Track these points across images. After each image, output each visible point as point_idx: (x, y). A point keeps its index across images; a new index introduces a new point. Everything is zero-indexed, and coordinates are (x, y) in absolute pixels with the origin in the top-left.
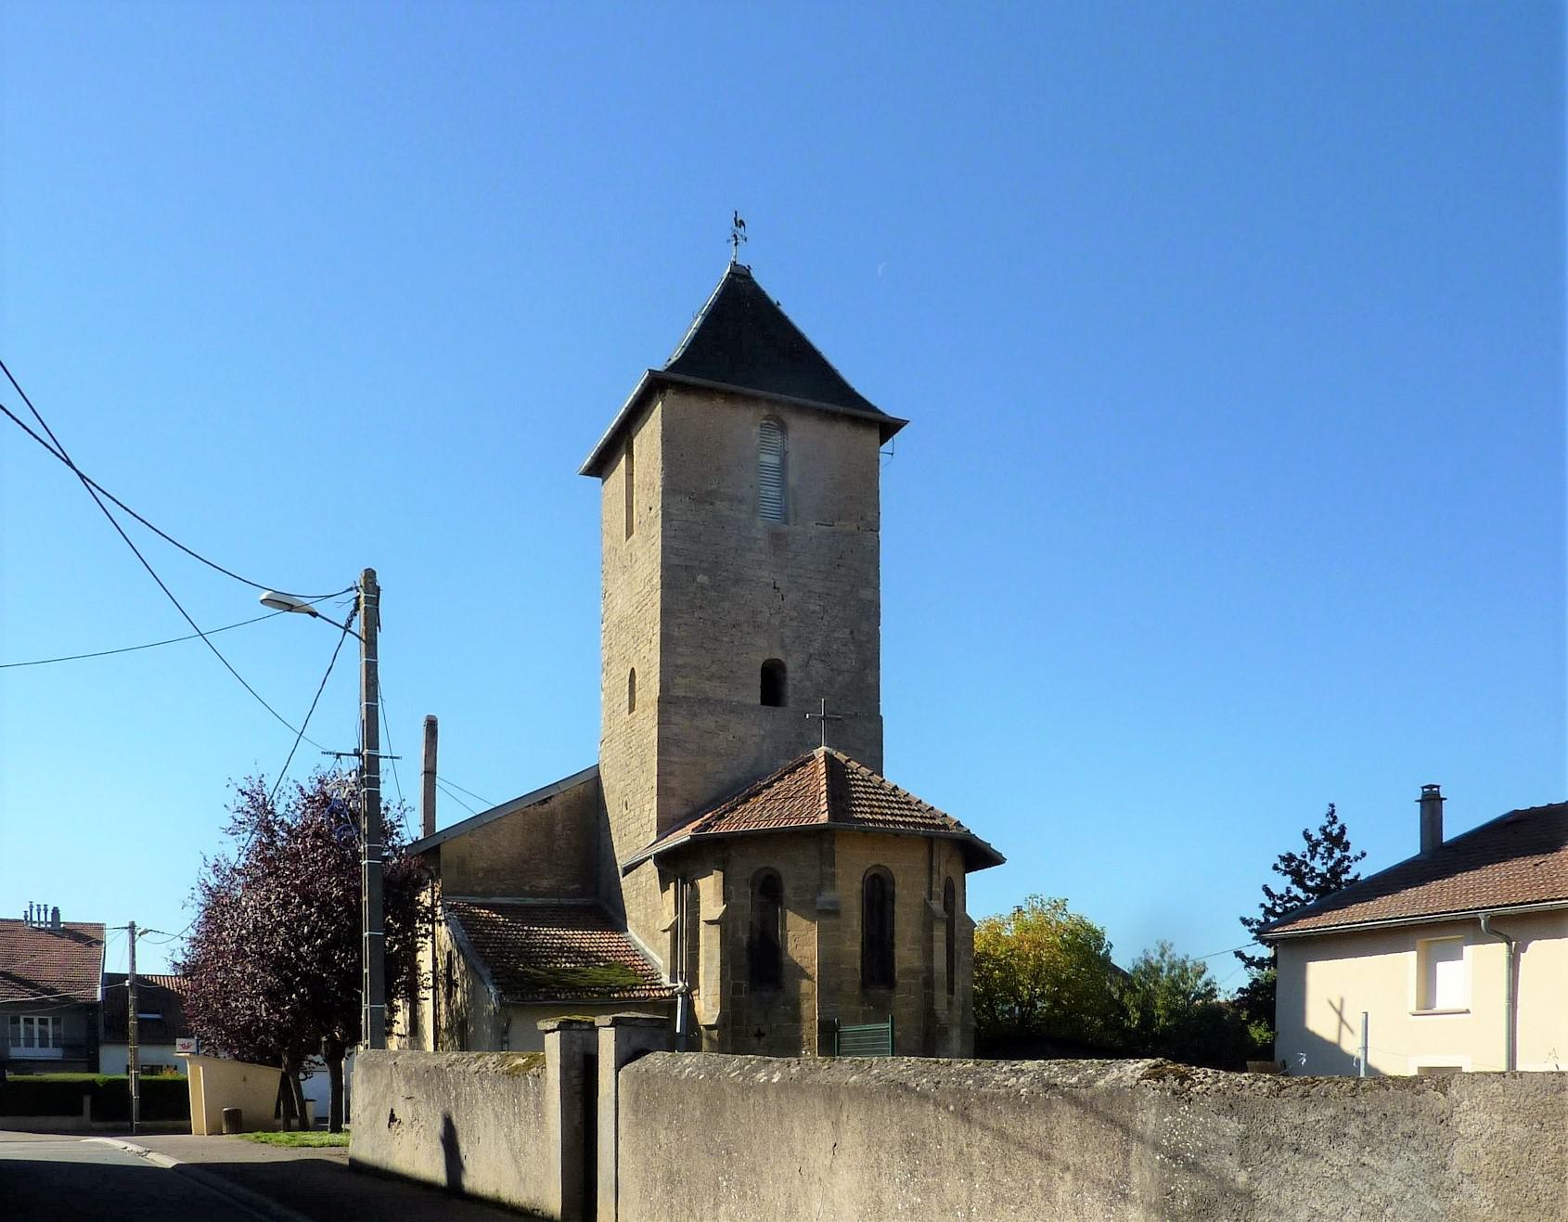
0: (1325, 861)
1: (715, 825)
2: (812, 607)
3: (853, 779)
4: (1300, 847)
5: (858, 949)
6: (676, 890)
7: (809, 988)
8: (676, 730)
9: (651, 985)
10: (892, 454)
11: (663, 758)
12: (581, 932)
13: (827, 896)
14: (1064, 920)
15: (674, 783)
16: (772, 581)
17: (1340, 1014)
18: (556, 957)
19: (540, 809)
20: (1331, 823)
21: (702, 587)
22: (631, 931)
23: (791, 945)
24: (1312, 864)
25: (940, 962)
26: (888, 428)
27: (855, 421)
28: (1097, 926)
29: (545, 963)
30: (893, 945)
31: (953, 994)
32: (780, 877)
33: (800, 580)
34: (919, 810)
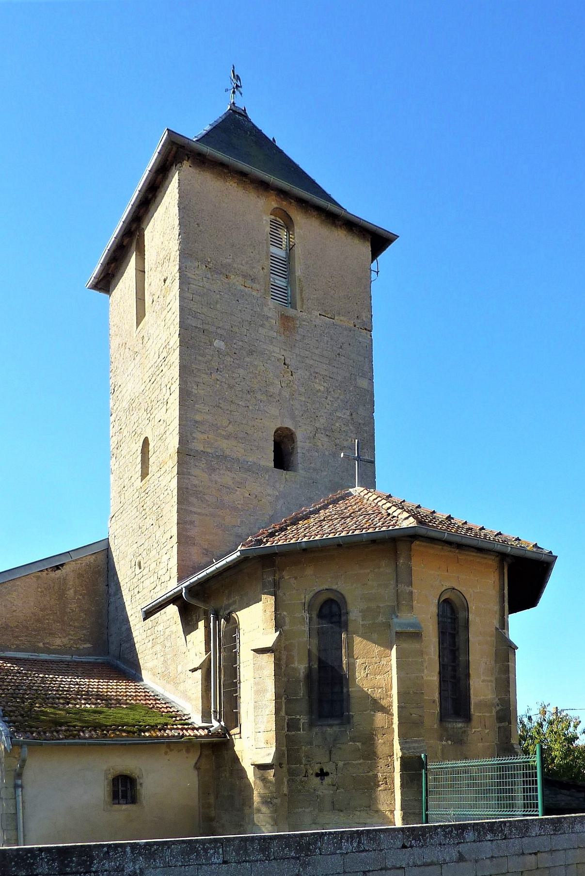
2: (318, 387)
6: (207, 627)
11: (184, 507)
12: (97, 681)
13: (405, 618)
15: (193, 532)
19: (53, 575)
23: (360, 674)
29: (63, 704)
32: (344, 598)
33: (307, 361)
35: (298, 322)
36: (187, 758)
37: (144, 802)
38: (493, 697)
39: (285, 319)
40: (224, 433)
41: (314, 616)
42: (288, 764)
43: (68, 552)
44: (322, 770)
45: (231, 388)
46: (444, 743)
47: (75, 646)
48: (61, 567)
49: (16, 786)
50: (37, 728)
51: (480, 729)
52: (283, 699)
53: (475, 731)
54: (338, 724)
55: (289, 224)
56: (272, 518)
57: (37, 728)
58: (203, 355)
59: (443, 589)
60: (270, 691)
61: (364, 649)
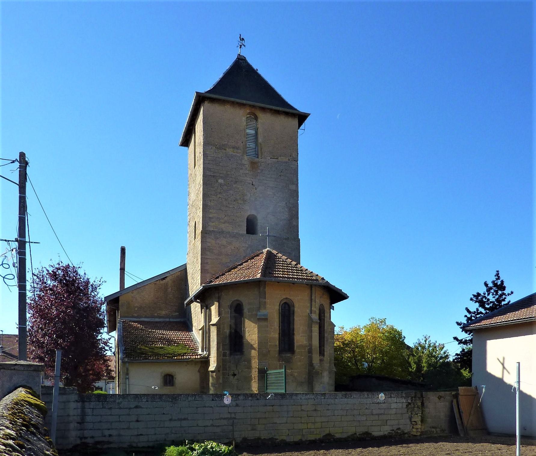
0: (494, 296)
1: (214, 281)
2: (269, 193)
3: (278, 261)
4: (482, 290)
5: (277, 336)
7: (254, 353)
8: (209, 244)
9: (193, 353)
10: (304, 130)
13: (263, 312)
14: (385, 327)
15: (208, 267)
16: (252, 182)
17: (503, 364)
18: (157, 342)
19: (162, 282)
20: (497, 279)
21: (221, 185)
22: (194, 332)
23: (247, 334)
24: (488, 297)
25: (316, 342)
26: (302, 118)
27: (287, 114)
28: (399, 329)
30: (294, 334)
31: (324, 355)
34: (306, 273)
35: (259, 164)
38: (306, 343)
40: (222, 221)
41: (233, 310)
42: (223, 370)
43: (169, 271)
46: (281, 362)
48: (165, 278)
49: (126, 379)
50: (134, 356)
51: (299, 357)
52: (221, 344)
53: (297, 358)
55: (256, 118)
56: (245, 257)
57: (134, 356)
58: (213, 187)
59: (282, 299)
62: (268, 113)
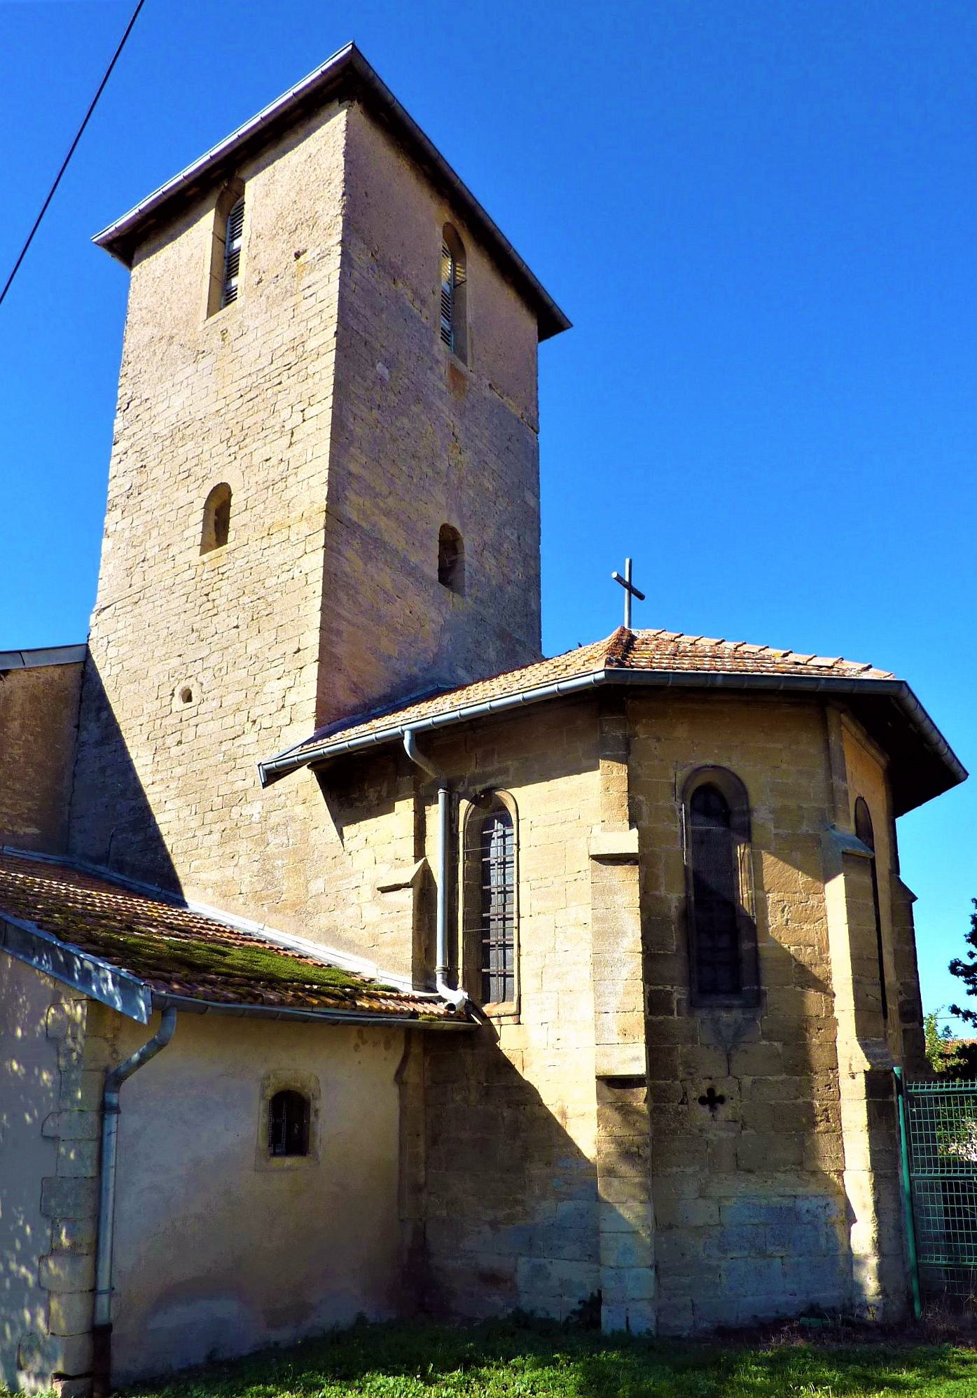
15: (341, 650)
23: (775, 920)
36: (385, 1059)
37: (320, 1153)
39: (455, 373)
43: (19, 652)
44: (711, 1091)
45: (394, 441)
47: (10, 828)
54: (741, 1007)
60: (630, 935)
61: (780, 878)
62: (485, 260)
